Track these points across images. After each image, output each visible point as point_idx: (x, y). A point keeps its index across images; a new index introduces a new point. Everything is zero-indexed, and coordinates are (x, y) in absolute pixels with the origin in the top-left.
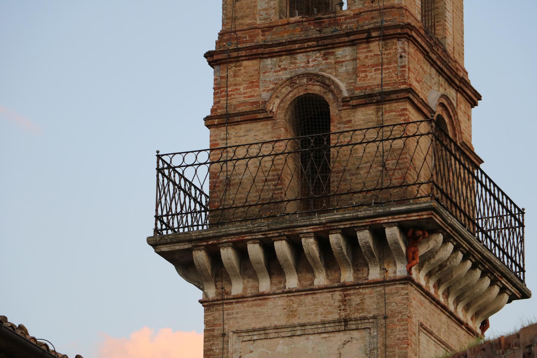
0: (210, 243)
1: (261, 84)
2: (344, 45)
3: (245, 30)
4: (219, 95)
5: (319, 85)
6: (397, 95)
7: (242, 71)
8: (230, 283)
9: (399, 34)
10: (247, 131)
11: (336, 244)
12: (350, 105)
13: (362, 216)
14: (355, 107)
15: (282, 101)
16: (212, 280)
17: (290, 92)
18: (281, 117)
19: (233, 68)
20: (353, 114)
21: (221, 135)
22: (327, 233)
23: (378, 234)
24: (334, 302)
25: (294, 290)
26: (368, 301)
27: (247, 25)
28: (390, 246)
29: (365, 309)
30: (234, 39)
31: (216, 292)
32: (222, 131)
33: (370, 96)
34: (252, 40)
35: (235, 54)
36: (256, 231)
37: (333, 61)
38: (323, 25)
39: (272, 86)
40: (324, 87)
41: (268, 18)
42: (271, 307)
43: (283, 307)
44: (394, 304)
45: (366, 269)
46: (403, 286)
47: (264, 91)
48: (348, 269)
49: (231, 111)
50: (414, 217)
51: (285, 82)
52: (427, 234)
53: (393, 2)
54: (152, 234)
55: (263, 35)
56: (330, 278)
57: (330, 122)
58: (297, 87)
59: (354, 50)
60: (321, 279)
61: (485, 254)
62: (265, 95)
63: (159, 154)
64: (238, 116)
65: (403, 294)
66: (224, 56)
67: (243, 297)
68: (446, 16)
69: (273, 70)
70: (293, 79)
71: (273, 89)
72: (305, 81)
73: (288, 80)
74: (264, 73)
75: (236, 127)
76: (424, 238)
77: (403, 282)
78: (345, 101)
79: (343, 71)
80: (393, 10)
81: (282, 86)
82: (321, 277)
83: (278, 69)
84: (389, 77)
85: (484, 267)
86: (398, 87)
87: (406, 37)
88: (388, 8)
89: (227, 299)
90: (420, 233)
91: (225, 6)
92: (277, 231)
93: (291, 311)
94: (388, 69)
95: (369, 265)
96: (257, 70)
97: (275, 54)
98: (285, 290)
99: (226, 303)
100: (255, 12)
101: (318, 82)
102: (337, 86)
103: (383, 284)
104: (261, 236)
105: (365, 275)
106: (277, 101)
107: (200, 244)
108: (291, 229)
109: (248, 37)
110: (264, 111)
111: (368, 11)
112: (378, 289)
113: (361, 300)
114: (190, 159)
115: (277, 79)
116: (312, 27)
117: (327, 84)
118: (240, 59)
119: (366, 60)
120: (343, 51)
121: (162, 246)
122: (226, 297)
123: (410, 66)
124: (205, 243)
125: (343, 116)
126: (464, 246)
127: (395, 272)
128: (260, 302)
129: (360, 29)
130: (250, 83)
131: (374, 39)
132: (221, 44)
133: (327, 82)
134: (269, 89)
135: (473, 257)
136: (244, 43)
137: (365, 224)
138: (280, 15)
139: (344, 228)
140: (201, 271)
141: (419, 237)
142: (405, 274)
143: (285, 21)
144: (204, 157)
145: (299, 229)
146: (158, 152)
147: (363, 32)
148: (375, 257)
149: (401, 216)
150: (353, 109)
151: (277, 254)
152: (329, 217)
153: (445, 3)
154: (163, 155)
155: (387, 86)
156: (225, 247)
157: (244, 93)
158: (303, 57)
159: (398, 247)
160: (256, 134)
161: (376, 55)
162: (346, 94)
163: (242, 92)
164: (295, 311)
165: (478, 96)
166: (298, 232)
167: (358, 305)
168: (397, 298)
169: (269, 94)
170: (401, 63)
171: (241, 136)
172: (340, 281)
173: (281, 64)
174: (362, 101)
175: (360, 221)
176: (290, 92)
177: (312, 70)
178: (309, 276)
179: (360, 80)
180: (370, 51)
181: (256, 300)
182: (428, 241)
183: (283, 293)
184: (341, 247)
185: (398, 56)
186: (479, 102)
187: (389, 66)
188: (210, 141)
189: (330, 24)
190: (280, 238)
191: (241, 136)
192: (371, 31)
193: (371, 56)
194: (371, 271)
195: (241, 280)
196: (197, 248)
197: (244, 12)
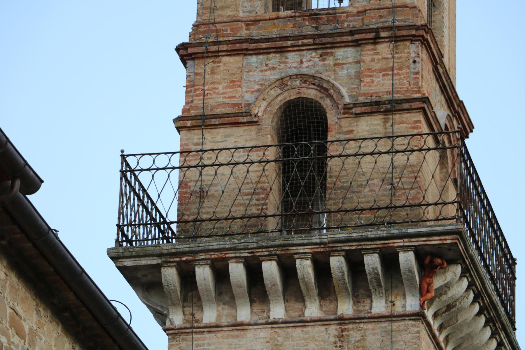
1: (244, 84)
2: (346, 44)
3: (226, 22)
4: (192, 94)
5: (315, 89)
6: (410, 104)
8: (201, 308)
9: (414, 36)
10: (225, 136)
11: (338, 268)
12: (352, 113)
13: (372, 236)
14: (358, 115)
15: (269, 104)
16: (180, 305)
17: (279, 95)
19: (211, 65)
20: (355, 124)
21: (193, 139)
22: (327, 255)
23: (390, 261)
24: (329, 337)
25: (280, 321)
26: (370, 338)
27: (228, 17)
28: (403, 275)
29: (366, 347)
30: (213, 31)
31: (183, 319)
32: (195, 134)
34: (234, 34)
36: (242, 247)
37: (331, 63)
38: (321, 22)
39: (257, 87)
40: (320, 91)
41: (252, 11)
42: (251, 339)
43: (266, 340)
44: (402, 343)
45: (369, 301)
46: (413, 323)
47: (247, 92)
48: (347, 300)
49: (208, 112)
50: (435, 241)
51: (275, 82)
52: (446, 264)
54: (113, 246)
55: (247, 30)
57: (327, 131)
58: (288, 90)
59: (358, 51)
60: (313, 310)
61: (493, 299)
62: (249, 97)
63: (124, 154)
64: (216, 118)
65: (414, 332)
66: (202, 49)
67: (217, 326)
68: (443, 32)
70: (284, 80)
71: (258, 90)
72: (298, 82)
73: (278, 80)
74: (248, 72)
75: (213, 131)
76: (441, 268)
77: (414, 318)
78: (347, 108)
79: (346, 73)
80: (405, 9)
81: (271, 87)
82: (314, 308)
83: (265, 68)
85: (489, 313)
86: (410, 96)
87: (420, 40)
88: (399, 7)
89: (198, 328)
90: (439, 261)
93: (276, 345)
94: (399, 74)
95: (373, 297)
96: (240, 67)
97: (262, 51)
99: (196, 332)
100: (237, 3)
101: (314, 84)
102: (339, 92)
103: (390, 319)
104: (247, 255)
105: (367, 308)
106: (264, 104)
107: (171, 260)
108: (285, 248)
109: (229, 30)
110: (249, 114)
111: (375, 9)
112: (383, 325)
113: (362, 336)
115: (263, 79)
116: (307, 23)
118: (220, 54)
119: (373, 63)
120: (344, 52)
121: (125, 260)
122: (196, 325)
123: (424, 74)
124: (178, 259)
125: (343, 125)
126: (478, 284)
127: (404, 306)
128: (237, 333)
129: (364, 27)
130: (230, 82)
132: (197, 36)
133: (325, 85)
134: (253, 90)
135: (483, 300)
138: (265, 10)
139: (350, 250)
140: (169, 292)
141: (436, 267)
142: (417, 309)
143: (274, 15)
144: (176, 160)
145: (294, 248)
146: (122, 151)
147: (370, 31)
148: (381, 286)
149: (420, 239)
150: (355, 117)
151: (264, 277)
152: (332, 236)
153: (443, 17)
154: (128, 156)
155: (397, 93)
157: (223, 93)
158: (296, 56)
159: (412, 276)
161: (384, 58)
162: (347, 100)
163: (221, 92)
164: (281, 345)
165: (471, 126)
166: (292, 252)
167: (358, 341)
168: (407, 336)
169: (253, 96)
170: (414, 69)
171: (218, 142)
172: (336, 314)
173: (268, 62)
174: (368, 109)
175: (370, 243)
176: (279, 95)
177: (307, 71)
178: (298, 305)
179: (364, 85)
180: (377, 54)
181: (233, 330)
182: (445, 272)
183: (267, 323)
184: (343, 272)
185: (411, 61)
186: (471, 135)
187: (400, 72)
188: (181, 146)
189: (329, 21)
190: (269, 257)
191: (218, 142)
192: (380, 30)
193: (378, 59)
194: (374, 304)
195: (215, 307)
196: (168, 264)
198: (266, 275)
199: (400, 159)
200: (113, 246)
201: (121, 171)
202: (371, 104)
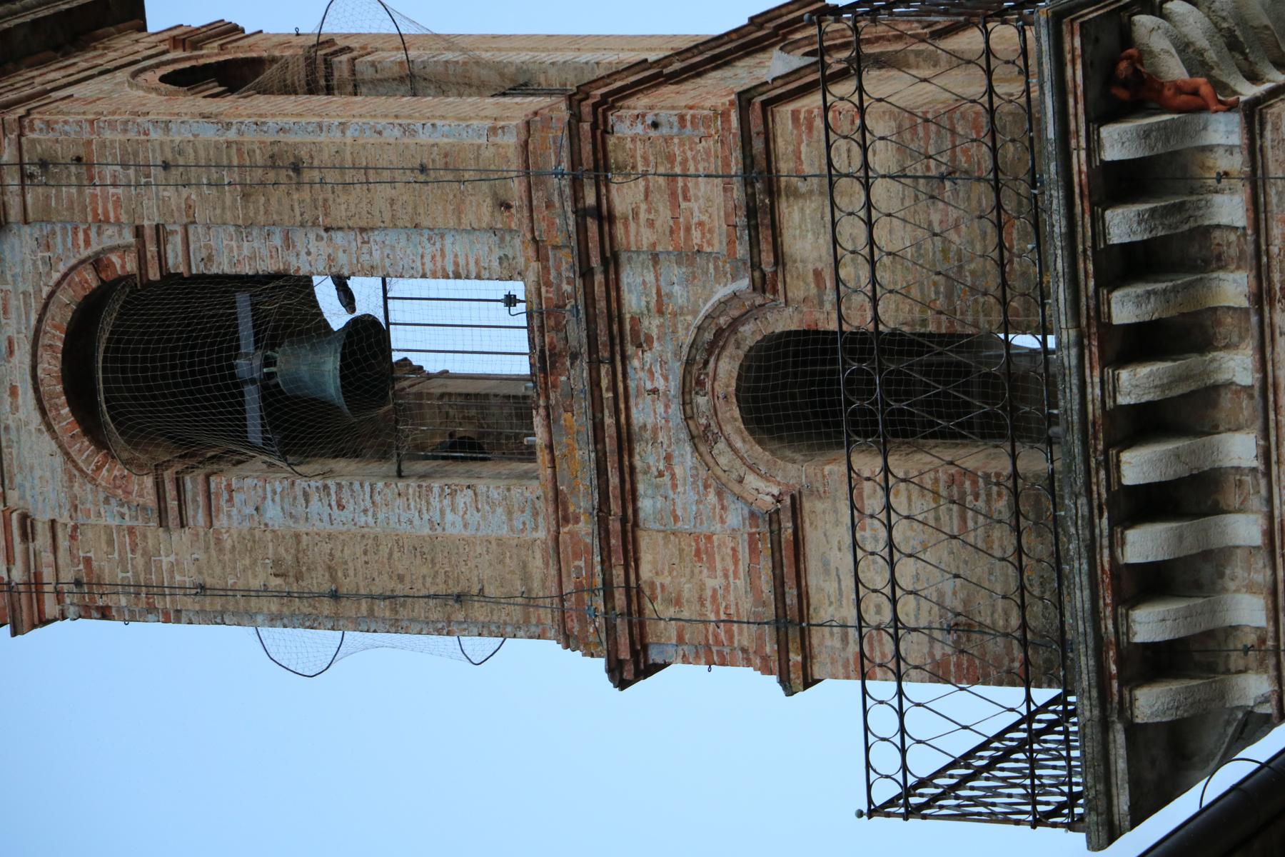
0: (1113, 669)
1: (704, 529)
2: (613, 286)
4: (726, 650)
5: (717, 360)
6: (754, 135)
7: (667, 580)
9: (594, 127)
10: (827, 572)
11: (1139, 305)
12: (775, 273)
13: (1063, 223)
14: (779, 258)
17: (730, 445)
18: (795, 470)
19: (659, 606)
20: (799, 265)
21: (833, 648)
22: (1106, 328)
25: (1262, 442)
27: (547, 564)
28: (1155, 152)
30: (580, 601)
31: (1257, 673)
33: (751, 212)
34: (587, 552)
35: (620, 599)
36: (1087, 532)
37: (657, 321)
38: (560, 345)
39: (712, 497)
40: (723, 348)
45: (1217, 233)
46: (1269, 127)
47: (723, 521)
48: (1214, 284)
49: (770, 613)
50: (1076, 74)
51: (701, 455)
53: (512, 149)
54: (1081, 838)
55: (577, 521)
56: (1235, 339)
57: (817, 332)
59: (630, 259)
60: (1237, 366)
62: (736, 516)
63: (865, 811)
64: (783, 594)
66: (622, 626)
68: (587, 63)
69: (670, 492)
70: (695, 432)
71: (719, 494)
72: (701, 400)
74: (676, 518)
76: (1141, 61)
77: (1257, 127)
78: (763, 284)
79: (678, 288)
80: (531, 147)
81: (712, 464)
82: (1231, 364)
84: (707, 160)
86: (734, 135)
87: (605, 111)
88: (526, 161)
90: (1123, 65)
91: (493, 628)
92: (1093, 473)
94: (684, 162)
95: (1207, 223)
98: (1261, 468)
100: (514, 542)
101: (706, 363)
103: (1260, 183)
104: (1105, 521)
105: (1233, 237)
106: (752, 480)
107: (1116, 699)
109: (577, 563)
110: (775, 517)
114: (883, 720)
115: (693, 483)
116: (563, 378)
117: (713, 339)
119: (658, 224)
120: (630, 291)
121: (1115, 809)
122: (1270, 643)
124: (1115, 684)
127: (1230, 149)
130: (700, 560)
131: (604, 201)
132: (591, 639)
133: (708, 336)
136: (592, 575)
137: (1087, 216)
140: (1192, 704)
141: (1137, 72)
142: (1236, 119)
144: (883, 688)
145: (1090, 408)
147: (581, 229)
148: (1183, 203)
149: (1071, 110)
150: (784, 265)
151: (1157, 480)
152: (1063, 318)
153: (553, 64)
154: (870, 801)
156: (1128, 627)
157: (726, 576)
158: (641, 406)
159: (1158, 130)
160: (835, 544)
161: (646, 196)
162: (744, 283)
166: (1099, 412)
171: (840, 589)
172: (1246, 311)
173: (654, 469)
174: (765, 234)
175: (1080, 229)
176: (730, 445)
178: (1226, 400)
179: (710, 244)
180: (636, 214)
183: (1268, 474)
184: (1149, 293)
185: (652, 133)
187: (679, 159)
189: (558, 328)
190: (1113, 468)
191: (840, 589)
192: (580, 206)
194: (1224, 220)
195: (1227, 597)
196: (1125, 709)
197: (513, 572)
198: (1154, 477)
199: (883, 158)
200: (1081, 838)
201: (906, 817)
202: (753, 228)
